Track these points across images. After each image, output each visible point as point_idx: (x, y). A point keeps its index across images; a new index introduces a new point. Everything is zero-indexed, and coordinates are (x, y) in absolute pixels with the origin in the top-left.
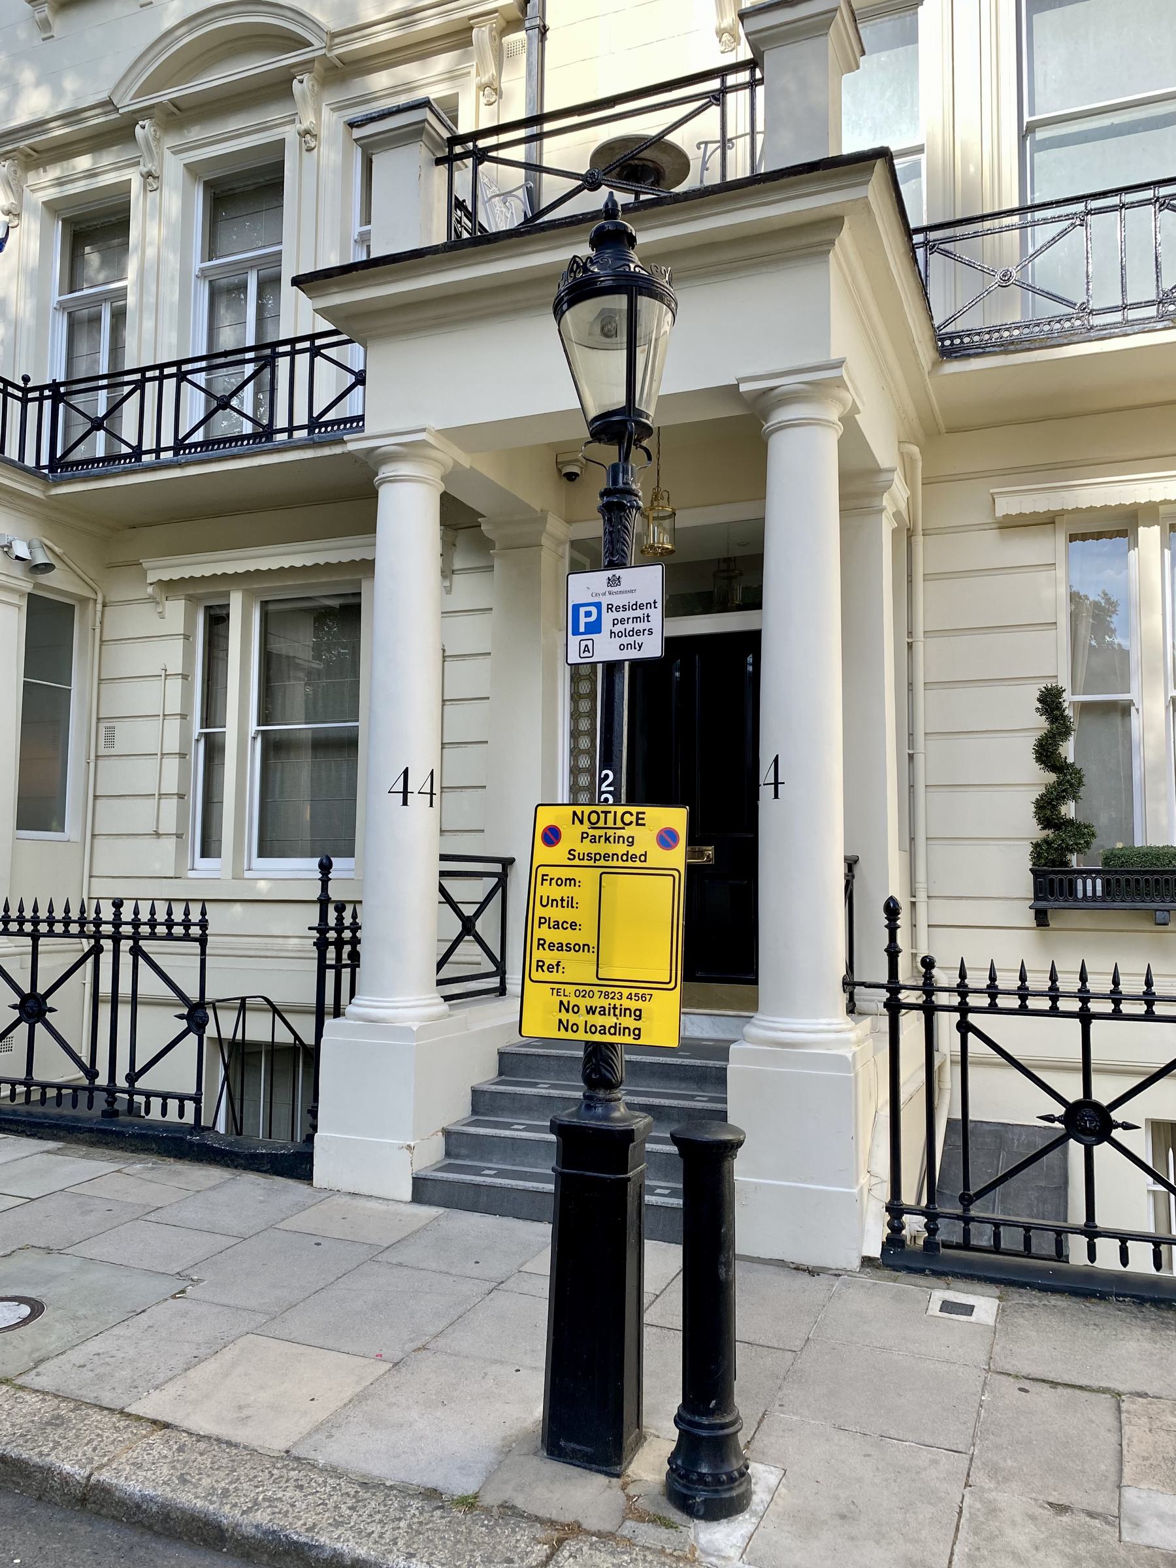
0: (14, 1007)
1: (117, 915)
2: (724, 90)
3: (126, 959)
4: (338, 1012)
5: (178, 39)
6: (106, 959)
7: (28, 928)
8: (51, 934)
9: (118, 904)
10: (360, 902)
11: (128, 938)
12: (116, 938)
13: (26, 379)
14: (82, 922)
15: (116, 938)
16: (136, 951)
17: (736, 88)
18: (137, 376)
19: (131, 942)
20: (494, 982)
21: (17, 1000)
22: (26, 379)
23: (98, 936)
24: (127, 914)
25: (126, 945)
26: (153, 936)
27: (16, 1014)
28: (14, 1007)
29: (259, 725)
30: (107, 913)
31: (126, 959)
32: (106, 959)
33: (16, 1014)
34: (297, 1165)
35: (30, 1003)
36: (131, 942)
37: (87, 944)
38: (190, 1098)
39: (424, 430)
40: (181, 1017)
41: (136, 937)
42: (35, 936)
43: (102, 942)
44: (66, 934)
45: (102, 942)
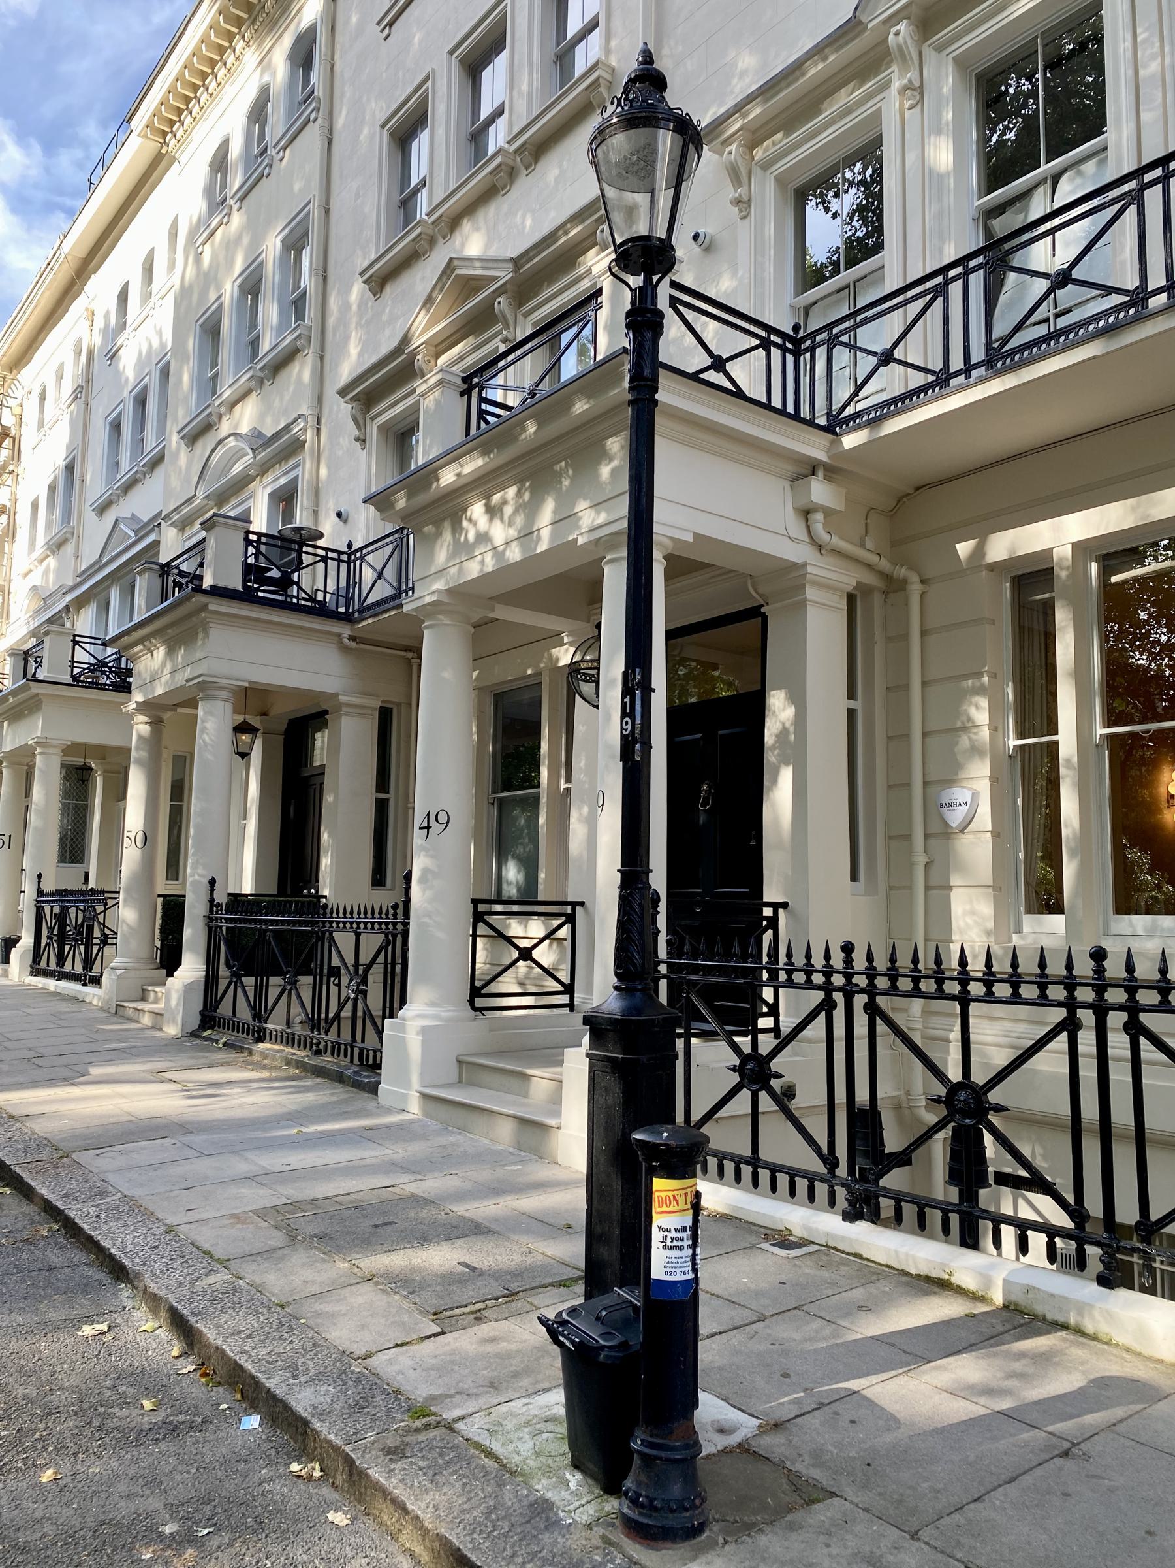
0: (734, 1069)
1: (848, 961)
2: (947, 282)
3: (1119, 1043)
4: (391, 1016)
5: (474, 268)
6: (839, 1015)
7: (952, 988)
8: (989, 997)
9: (848, 948)
10: (582, 904)
11: (862, 991)
12: (1101, 1010)
13: (350, 545)
14: (828, 973)
15: (1101, 1010)
16: (872, 1010)
17: (955, 279)
18: (322, 553)
19: (1124, 1016)
20: (565, 999)
21: (736, 1061)
22: (350, 545)
23: (828, 988)
24: (860, 963)
25: (860, 1000)
26: (894, 991)
27: (735, 1078)
28: (734, 1069)
29: (388, 800)
30: (838, 961)
31: (1119, 1043)
32: (839, 1015)
33: (735, 1078)
34: (373, 1089)
35: (750, 1065)
36: (1124, 1016)
37: (1060, 1014)
38: (747, 1163)
39: (201, 675)
40: (778, 1076)
41: (871, 991)
42: (964, 1000)
43: (1080, 1013)
44: (1016, 999)
45: (1080, 1013)
